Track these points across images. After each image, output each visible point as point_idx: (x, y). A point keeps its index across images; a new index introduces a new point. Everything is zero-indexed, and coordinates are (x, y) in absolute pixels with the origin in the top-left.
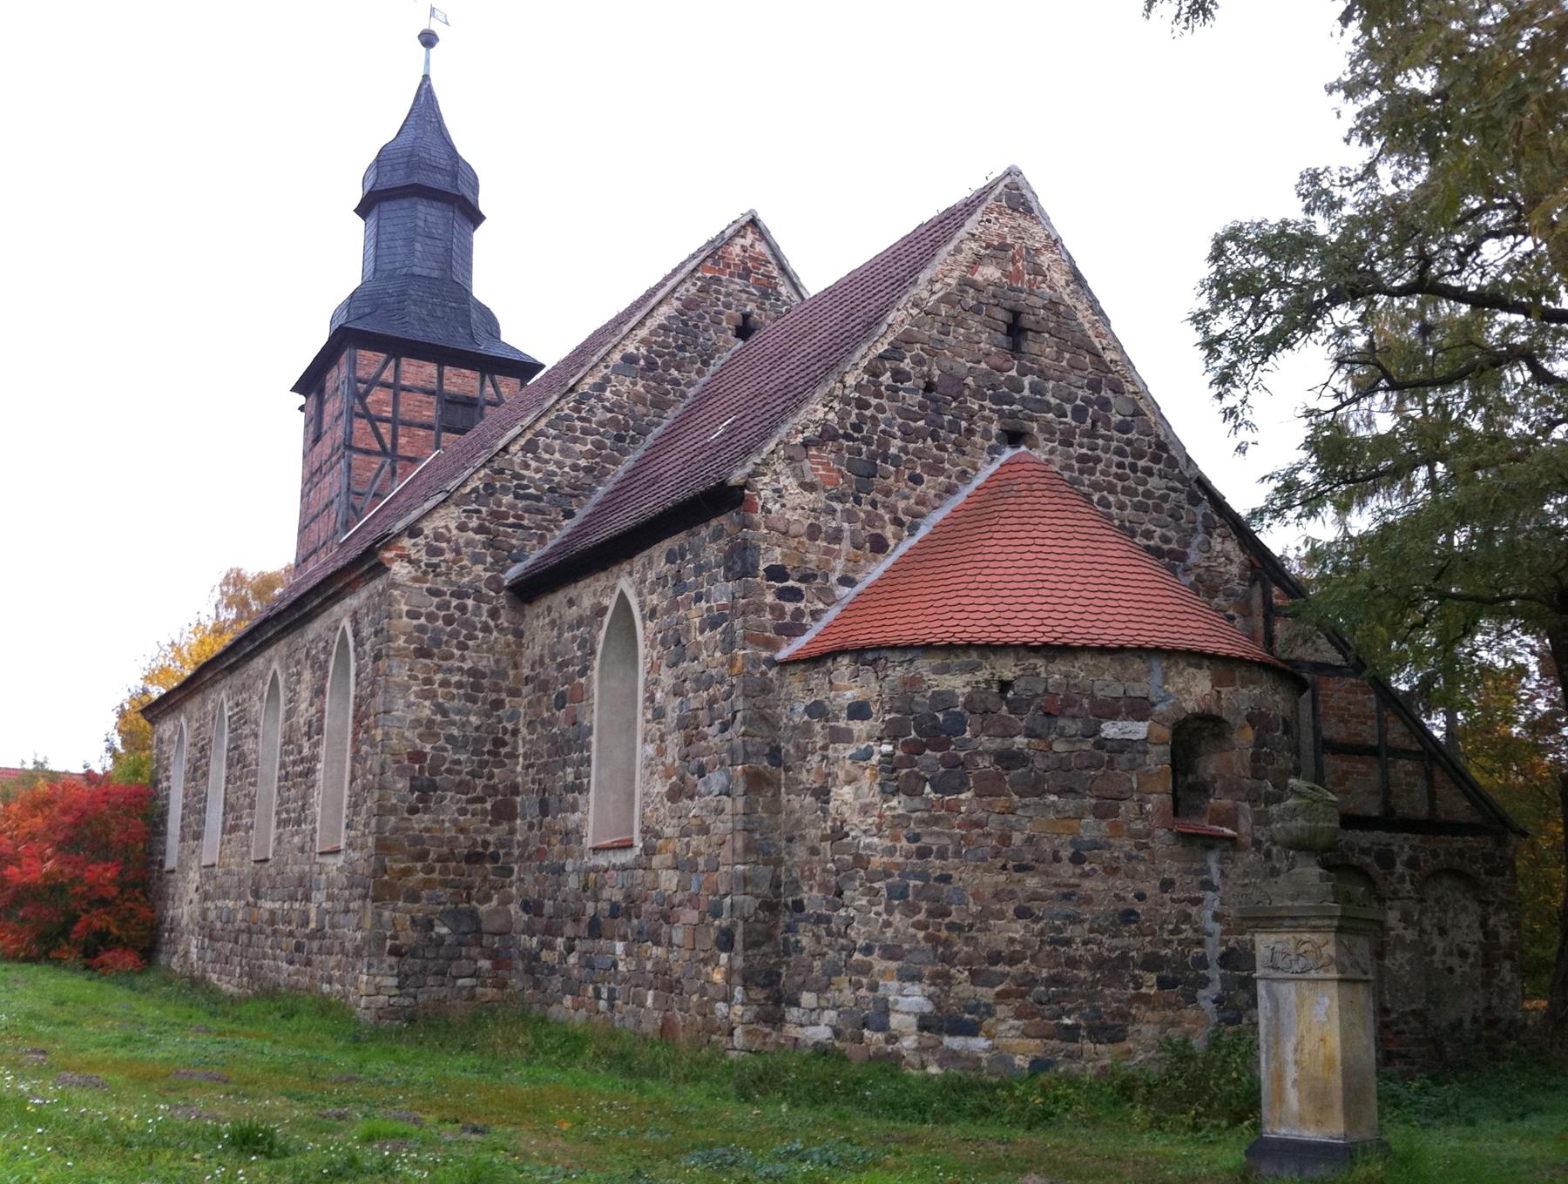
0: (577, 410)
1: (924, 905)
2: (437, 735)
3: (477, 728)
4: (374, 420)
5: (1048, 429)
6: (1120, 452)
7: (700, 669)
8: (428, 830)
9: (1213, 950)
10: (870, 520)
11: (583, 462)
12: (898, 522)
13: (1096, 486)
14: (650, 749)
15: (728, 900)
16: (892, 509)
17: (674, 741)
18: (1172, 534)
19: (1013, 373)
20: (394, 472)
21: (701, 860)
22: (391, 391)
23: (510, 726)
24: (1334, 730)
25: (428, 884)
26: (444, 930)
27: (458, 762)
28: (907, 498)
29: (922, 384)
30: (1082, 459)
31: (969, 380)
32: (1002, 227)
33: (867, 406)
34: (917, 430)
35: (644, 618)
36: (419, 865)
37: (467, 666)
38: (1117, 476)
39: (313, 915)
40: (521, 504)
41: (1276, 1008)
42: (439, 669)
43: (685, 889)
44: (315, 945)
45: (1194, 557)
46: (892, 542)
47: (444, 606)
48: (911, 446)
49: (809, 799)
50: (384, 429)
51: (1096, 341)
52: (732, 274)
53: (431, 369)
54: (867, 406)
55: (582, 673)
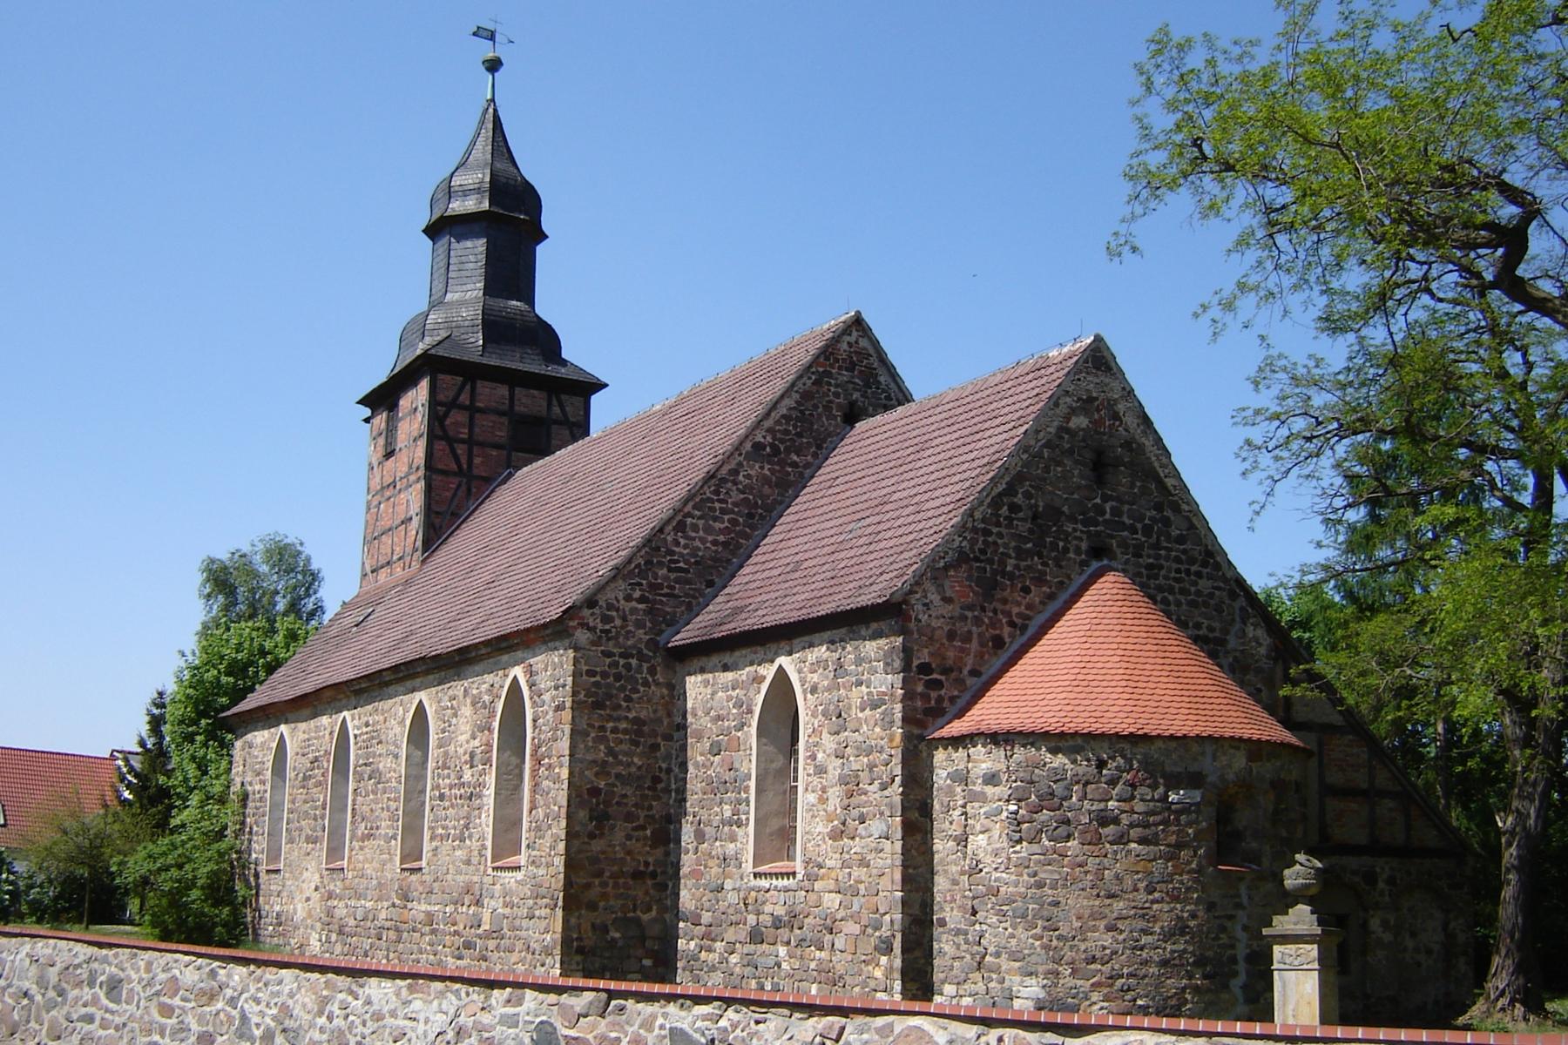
0: (717, 492)
1: (1040, 923)
2: (608, 774)
3: (639, 768)
4: (451, 441)
5: (1123, 544)
6: (1178, 560)
7: (861, 739)
8: (603, 852)
9: (1241, 951)
10: (993, 625)
11: (721, 538)
12: (1012, 624)
13: (1160, 589)
14: (812, 798)
15: (887, 917)
16: (1009, 614)
17: (835, 796)
18: (1217, 625)
19: (1098, 501)
20: (469, 490)
21: (862, 887)
22: (467, 414)
23: (664, 766)
24: (1335, 777)
25: (604, 896)
26: (617, 935)
27: (625, 796)
28: (1019, 604)
29: (1030, 514)
30: (1150, 567)
31: (1065, 509)
32: (1090, 384)
33: (989, 533)
34: (1028, 551)
35: (805, 692)
36: (597, 882)
37: (631, 716)
38: (1175, 579)
39: (486, 917)
40: (672, 576)
41: (1284, 986)
42: (610, 718)
43: (847, 908)
44: (492, 944)
45: (1232, 642)
46: (1007, 640)
47: (615, 664)
48: (1023, 564)
49: (951, 843)
50: (461, 450)
51: (1160, 470)
52: (840, 368)
53: (503, 391)
54: (989, 533)
55: (740, 727)
